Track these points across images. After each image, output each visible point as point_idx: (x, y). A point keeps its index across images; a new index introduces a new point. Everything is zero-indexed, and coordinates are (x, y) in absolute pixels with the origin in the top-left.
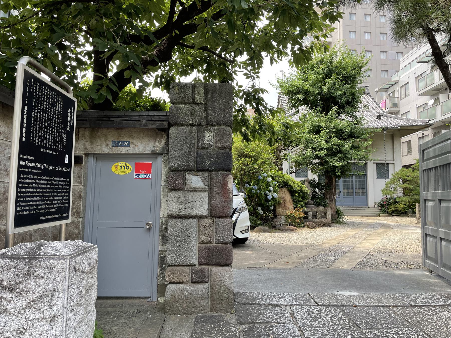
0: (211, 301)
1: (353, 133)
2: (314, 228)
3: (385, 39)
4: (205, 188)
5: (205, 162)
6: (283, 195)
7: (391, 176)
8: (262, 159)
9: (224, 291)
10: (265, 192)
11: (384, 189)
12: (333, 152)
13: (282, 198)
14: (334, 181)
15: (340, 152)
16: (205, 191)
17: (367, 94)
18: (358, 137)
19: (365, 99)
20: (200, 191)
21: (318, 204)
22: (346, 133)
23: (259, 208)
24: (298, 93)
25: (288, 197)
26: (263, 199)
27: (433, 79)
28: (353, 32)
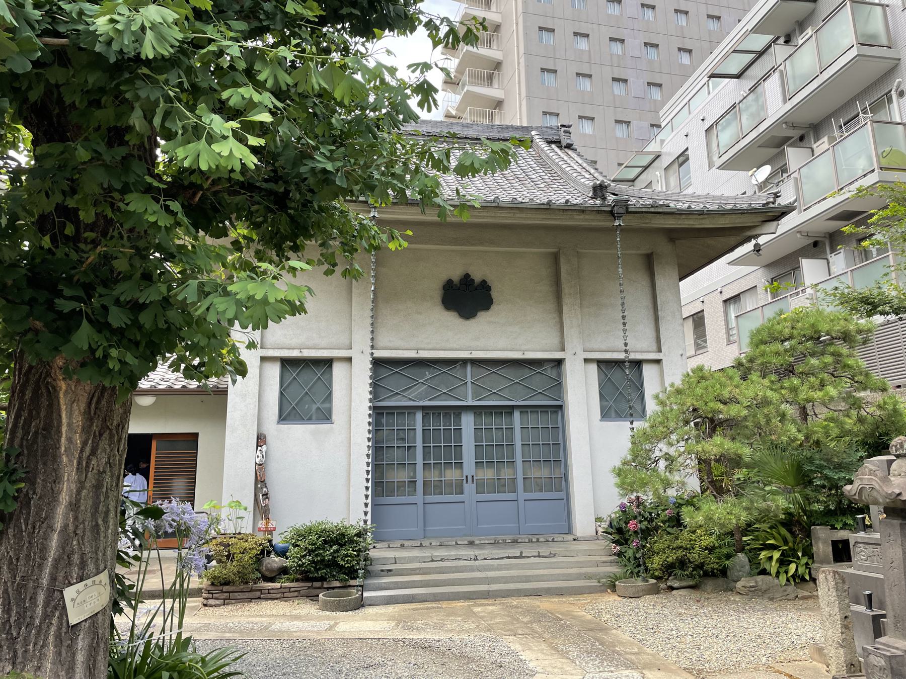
3: (623, 93)
7: (651, 406)
11: (625, 463)
17: (569, 146)
28: (549, 71)
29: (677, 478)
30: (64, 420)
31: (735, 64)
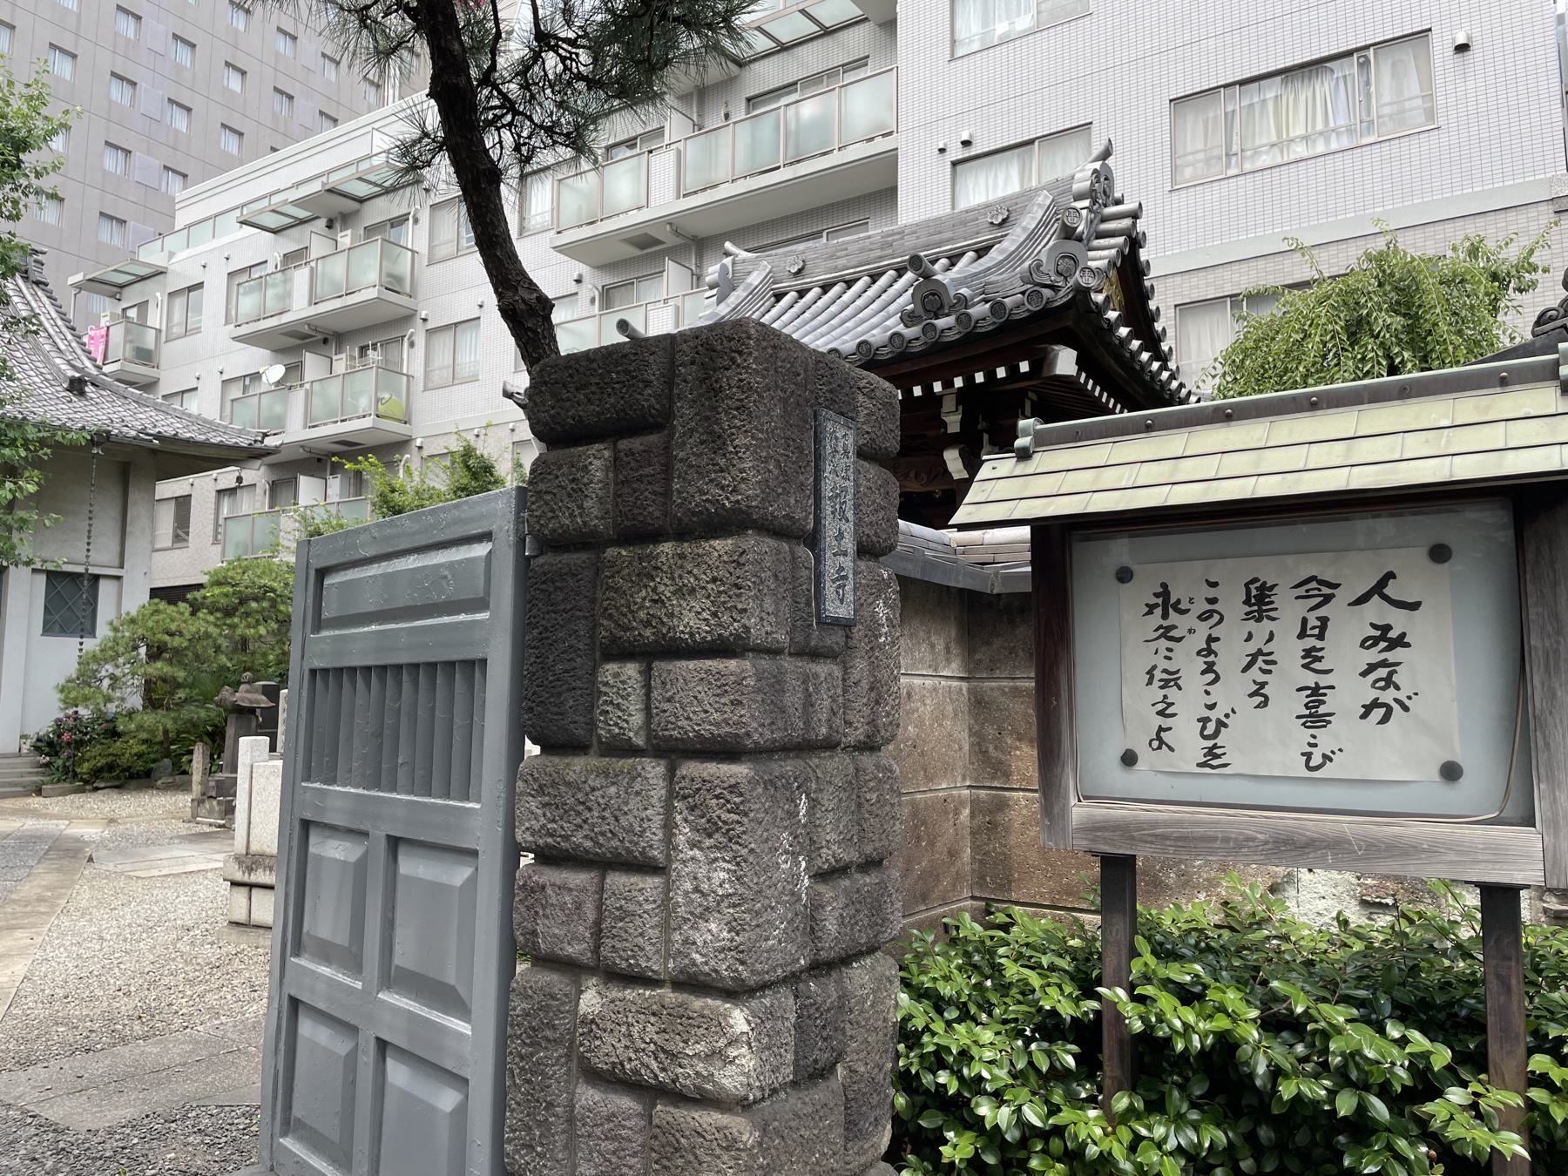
3: (126, 102)
7: (103, 630)
17: (38, 283)
27: (288, 295)
29: (118, 694)
30: (337, 304)
31: (274, 221)
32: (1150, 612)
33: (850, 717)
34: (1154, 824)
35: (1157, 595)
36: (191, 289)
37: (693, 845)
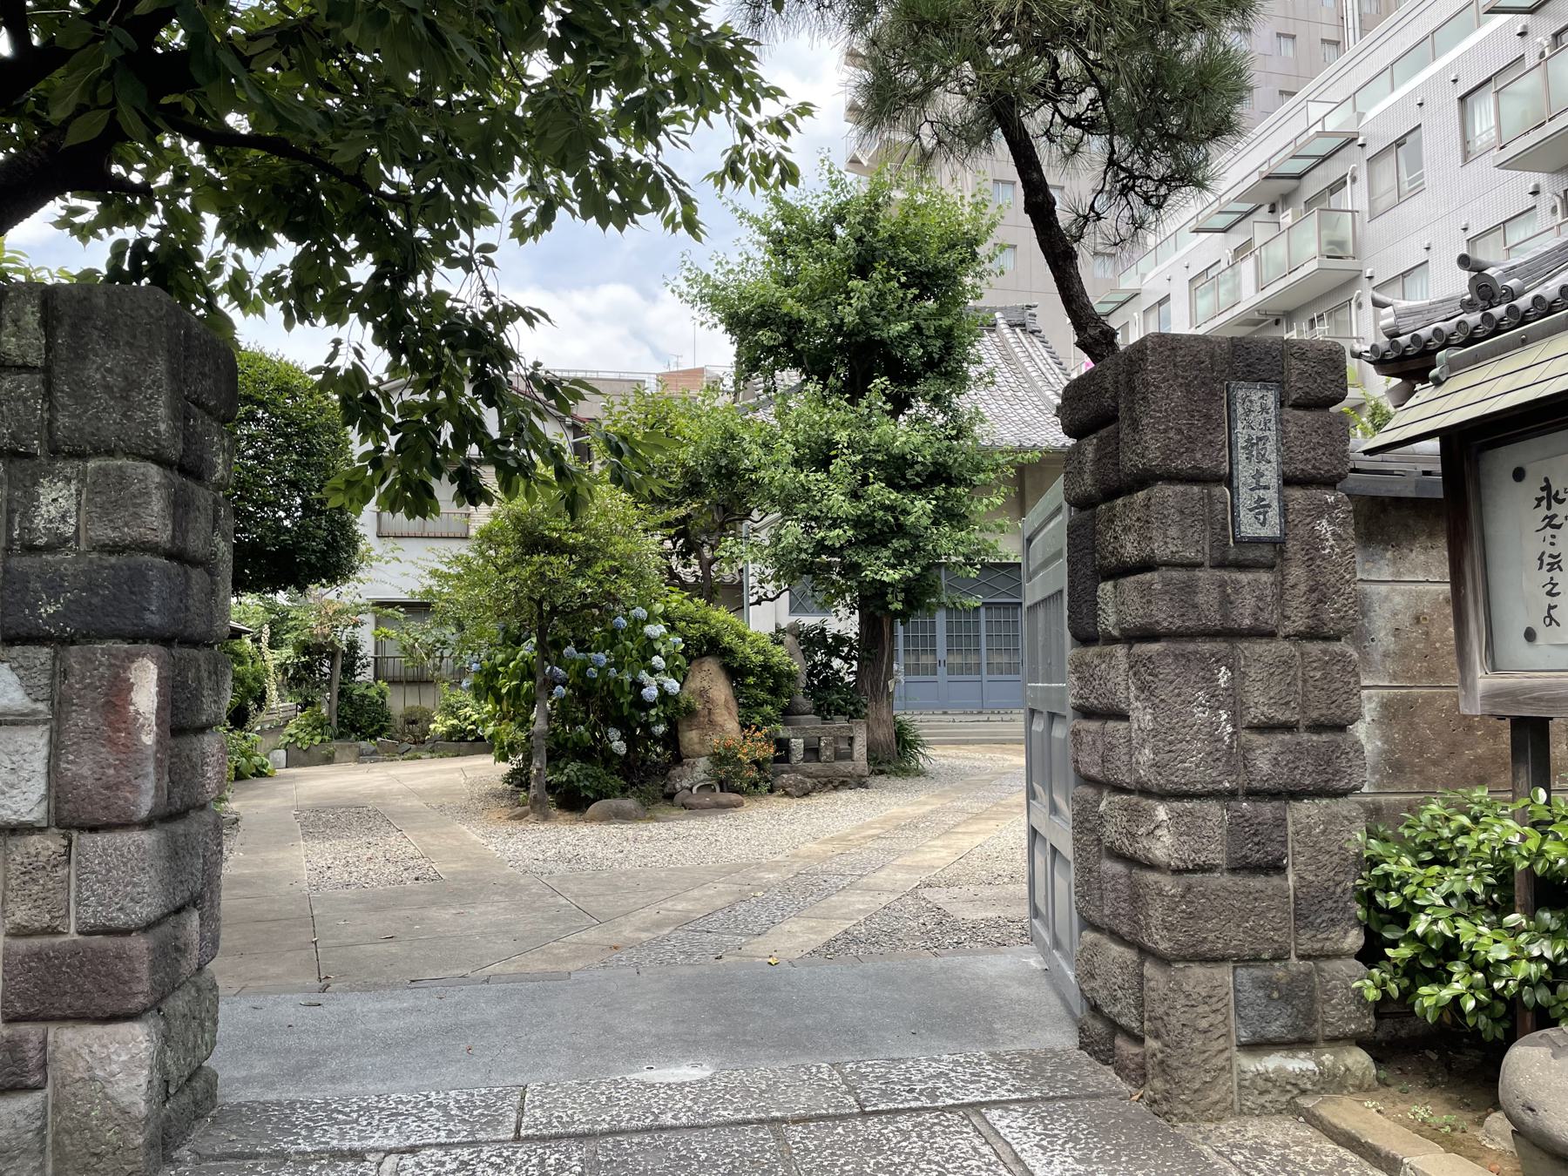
0: (55, 1161)
1: (944, 465)
2: (806, 794)
4: (34, 712)
5: (34, 607)
6: (705, 684)
8: (613, 558)
9: (106, 1118)
10: (635, 673)
12: (875, 532)
13: (702, 693)
14: (886, 630)
15: (900, 530)
16: (36, 723)
17: (1032, 332)
18: (961, 481)
19: (986, 349)
20: (14, 723)
21: (824, 710)
22: (918, 467)
23: (614, 734)
24: (762, 324)
25: (721, 691)
26: (625, 700)
27: (1237, 288)
30: (1282, 284)
32: (1538, 505)
33: (1288, 613)
34: (1532, 689)
35: (1542, 489)
36: (1160, 303)
37: (1137, 698)
